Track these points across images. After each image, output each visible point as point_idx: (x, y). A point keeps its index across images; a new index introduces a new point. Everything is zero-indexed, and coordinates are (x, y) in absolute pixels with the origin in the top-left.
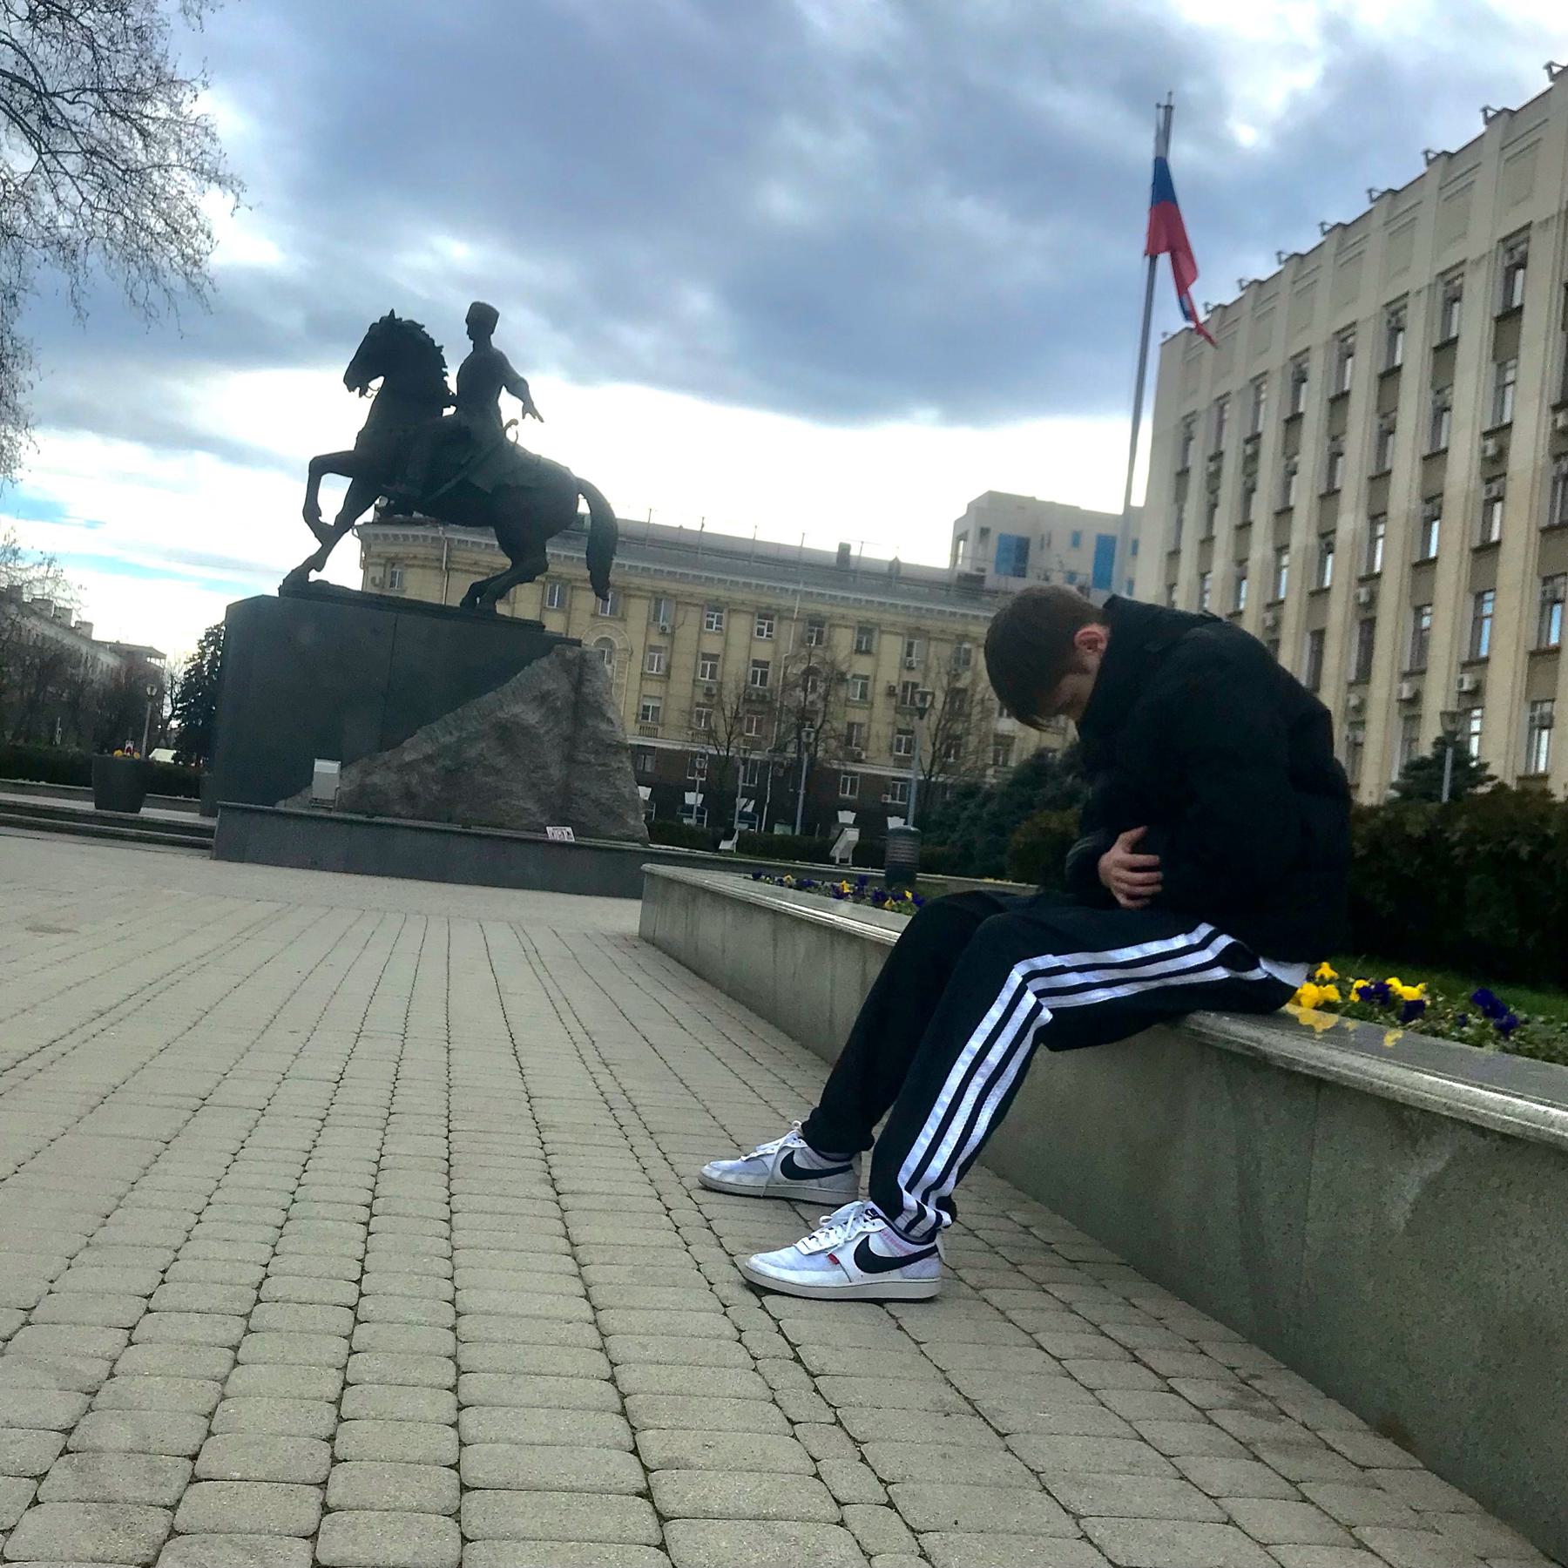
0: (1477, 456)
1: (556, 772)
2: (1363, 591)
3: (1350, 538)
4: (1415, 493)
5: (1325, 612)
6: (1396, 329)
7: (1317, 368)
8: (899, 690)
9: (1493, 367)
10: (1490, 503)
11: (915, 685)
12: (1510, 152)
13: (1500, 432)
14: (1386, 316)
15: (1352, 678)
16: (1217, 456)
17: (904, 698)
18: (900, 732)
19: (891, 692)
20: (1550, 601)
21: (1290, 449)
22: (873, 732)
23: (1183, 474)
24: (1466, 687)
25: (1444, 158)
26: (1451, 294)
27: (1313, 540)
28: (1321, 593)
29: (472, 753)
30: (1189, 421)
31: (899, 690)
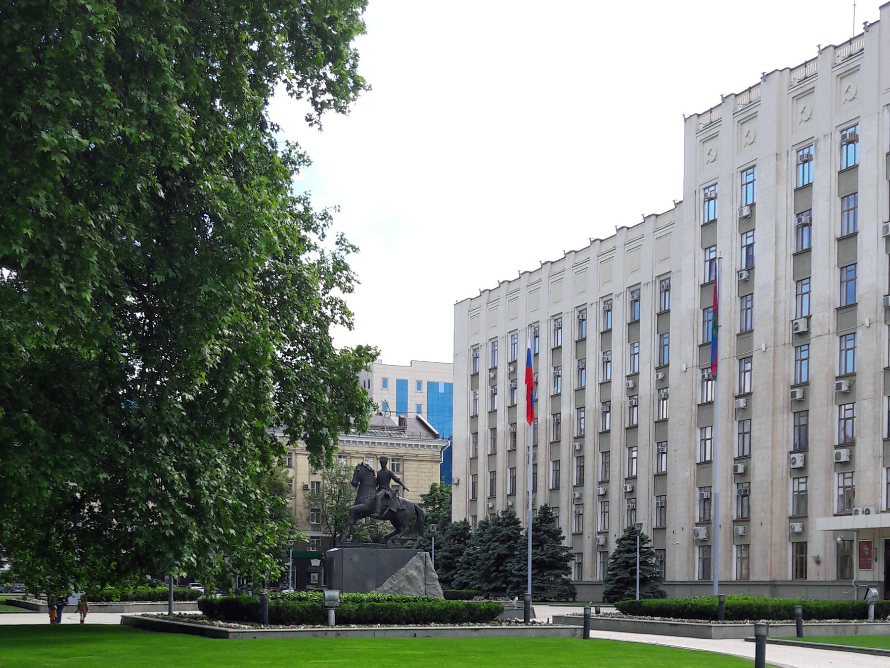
0: (625, 387)
1: (423, 588)
2: (577, 444)
3: (568, 418)
4: (598, 400)
5: (495, 463)
6: (608, 311)
7: (545, 331)
8: (310, 487)
9: (657, 336)
10: (605, 413)
11: (318, 483)
12: (628, 247)
13: (634, 376)
14: (577, 314)
15: (575, 484)
16: (494, 369)
17: (313, 491)
18: (313, 510)
19: (305, 488)
20: (661, 453)
21: (633, 337)
22: (298, 512)
23: (475, 375)
24: (628, 490)
25: (654, 217)
26: (607, 308)
27: (599, 405)
28: (606, 433)
29: (401, 586)
30: (475, 349)
31: (310, 487)
